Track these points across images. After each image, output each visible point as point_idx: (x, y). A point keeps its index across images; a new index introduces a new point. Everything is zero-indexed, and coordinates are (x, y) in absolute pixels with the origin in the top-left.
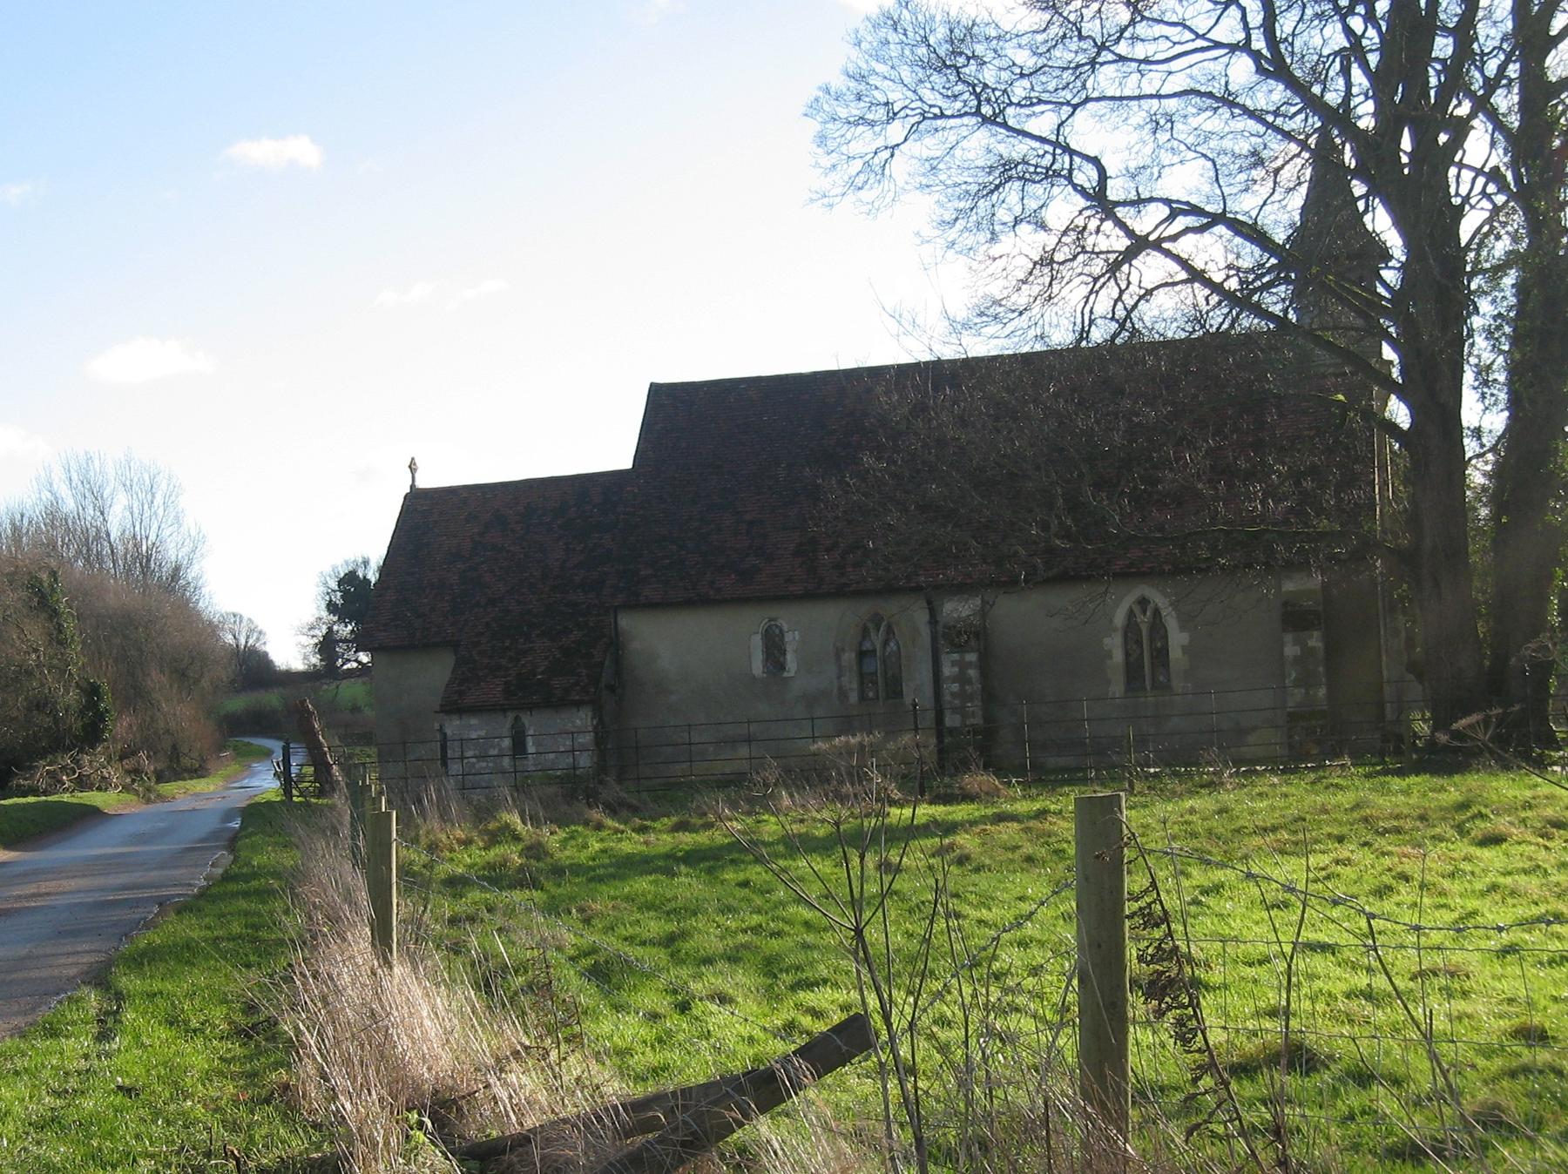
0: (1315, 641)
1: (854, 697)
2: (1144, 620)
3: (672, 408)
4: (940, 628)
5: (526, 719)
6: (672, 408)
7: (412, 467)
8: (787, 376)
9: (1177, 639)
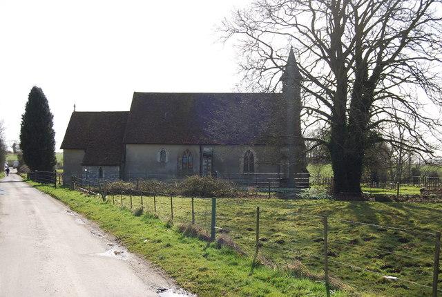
3: (139, 98)
6: (139, 98)
7: (75, 106)
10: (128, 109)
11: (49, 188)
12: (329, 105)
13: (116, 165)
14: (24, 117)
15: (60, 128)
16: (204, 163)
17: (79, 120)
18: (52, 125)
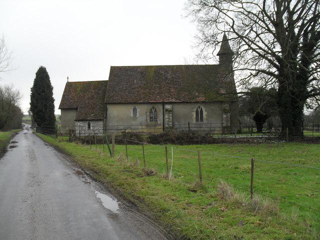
0: (229, 115)
1: (149, 121)
2: (199, 110)
3: (115, 71)
4: (165, 110)
5: (91, 123)
6: (115, 71)
7: (68, 78)
8: (173, 66)
9: (205, 113)
10: (107, 79)
11: (49, 138)
12: (275, 66)
13: (100, 120)
14: (32, 89)
15: (58, 95)
16: (166, 117)
17: (70, 86)
18: (52, 94)
